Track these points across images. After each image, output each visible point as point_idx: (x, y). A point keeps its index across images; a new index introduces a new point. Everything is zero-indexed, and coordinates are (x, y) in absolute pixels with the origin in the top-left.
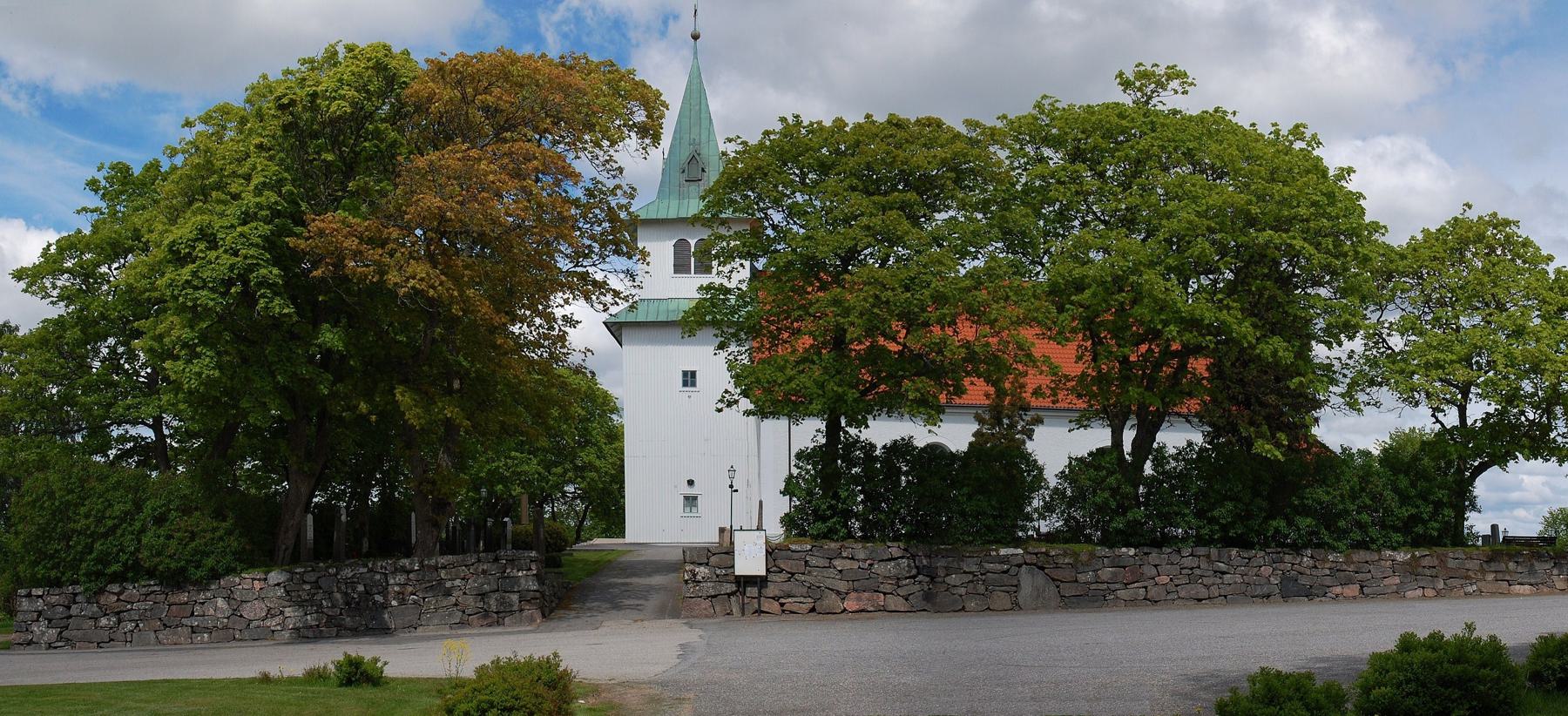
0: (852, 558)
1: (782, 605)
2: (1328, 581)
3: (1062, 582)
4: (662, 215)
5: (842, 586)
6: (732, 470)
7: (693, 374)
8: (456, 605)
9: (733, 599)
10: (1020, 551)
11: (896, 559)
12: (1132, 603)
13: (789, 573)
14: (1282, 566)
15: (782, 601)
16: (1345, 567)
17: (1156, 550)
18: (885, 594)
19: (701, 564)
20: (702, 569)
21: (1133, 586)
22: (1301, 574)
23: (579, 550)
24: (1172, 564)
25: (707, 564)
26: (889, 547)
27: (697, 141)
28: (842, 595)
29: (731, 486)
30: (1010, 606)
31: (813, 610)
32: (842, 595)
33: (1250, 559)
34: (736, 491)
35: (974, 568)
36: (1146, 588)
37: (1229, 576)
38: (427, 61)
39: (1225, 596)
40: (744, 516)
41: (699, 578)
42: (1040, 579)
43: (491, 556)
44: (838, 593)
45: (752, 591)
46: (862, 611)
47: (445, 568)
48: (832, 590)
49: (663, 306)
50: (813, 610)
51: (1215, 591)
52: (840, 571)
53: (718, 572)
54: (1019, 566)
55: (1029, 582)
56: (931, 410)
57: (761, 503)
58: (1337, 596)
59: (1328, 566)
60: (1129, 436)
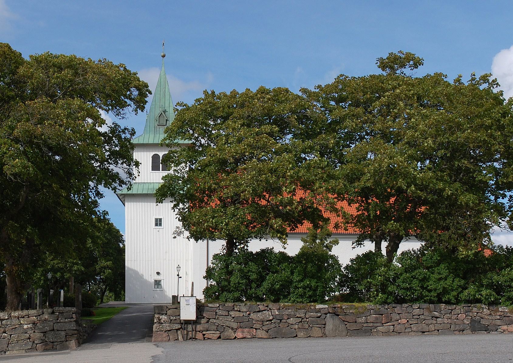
0: (240, 311)
1: (204, 335)
2: (498, 322)
3: (348, 322)
4: (146, 142)
5: (235, 325)
6: (179, 267)
7: (161, 220)
8: (29, 338)
9: (179, 332)
10: (326, 306)
11: (262, 311)
12: (387, 334)
13: (208, 318)
14: (471, 314)
15: (204, 333)
16: (509, 315)
17: (399, 305)
18: (256, 329)
19: (163, 314)
20: (163, 316)
21: (387, 324)
22: (482, 318)
23: (102, 307)
24: (408, 312)
25: (166, 314)
26: (258, 305)
27: (164, 106)
28: (235, 330)
29: (178, 275)
30: (321, 335)
31: (219, 337)
32: (235, 330)
33: (452, 310)
34: (181, 277)
35: (303, 315)
36: (394, 325)
37: (441, 319)
38: (31, 57)
39: (438, 330)
40: (184, 290)
41: (162, 321)
42: (337, 320)
43: (50, 310)
44: (232, 329)
45: (190, 327)
46: (245, 338)
47: (24, 317)
48: (229, 327)
49: (146, 186)
50: (219, 337)
51: (432, 327)
52: (233, 317)
53: (172, 318)
54: (326, 314)
55: (331, 322)
56: (282, 235)
57: (193, 283)
58: (504, 331)
59: (498, 314)
60: (384, 245)
